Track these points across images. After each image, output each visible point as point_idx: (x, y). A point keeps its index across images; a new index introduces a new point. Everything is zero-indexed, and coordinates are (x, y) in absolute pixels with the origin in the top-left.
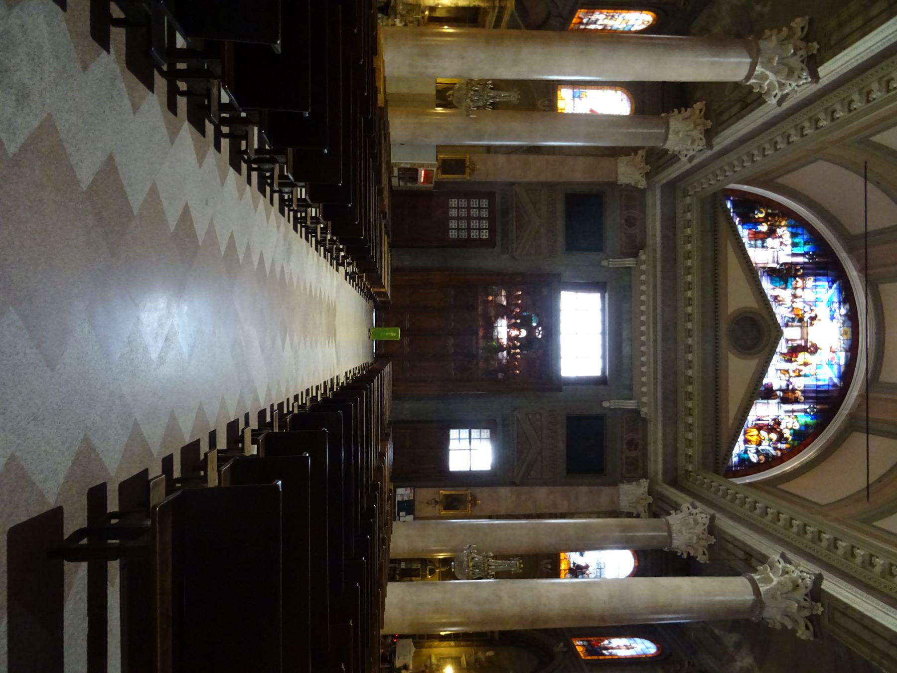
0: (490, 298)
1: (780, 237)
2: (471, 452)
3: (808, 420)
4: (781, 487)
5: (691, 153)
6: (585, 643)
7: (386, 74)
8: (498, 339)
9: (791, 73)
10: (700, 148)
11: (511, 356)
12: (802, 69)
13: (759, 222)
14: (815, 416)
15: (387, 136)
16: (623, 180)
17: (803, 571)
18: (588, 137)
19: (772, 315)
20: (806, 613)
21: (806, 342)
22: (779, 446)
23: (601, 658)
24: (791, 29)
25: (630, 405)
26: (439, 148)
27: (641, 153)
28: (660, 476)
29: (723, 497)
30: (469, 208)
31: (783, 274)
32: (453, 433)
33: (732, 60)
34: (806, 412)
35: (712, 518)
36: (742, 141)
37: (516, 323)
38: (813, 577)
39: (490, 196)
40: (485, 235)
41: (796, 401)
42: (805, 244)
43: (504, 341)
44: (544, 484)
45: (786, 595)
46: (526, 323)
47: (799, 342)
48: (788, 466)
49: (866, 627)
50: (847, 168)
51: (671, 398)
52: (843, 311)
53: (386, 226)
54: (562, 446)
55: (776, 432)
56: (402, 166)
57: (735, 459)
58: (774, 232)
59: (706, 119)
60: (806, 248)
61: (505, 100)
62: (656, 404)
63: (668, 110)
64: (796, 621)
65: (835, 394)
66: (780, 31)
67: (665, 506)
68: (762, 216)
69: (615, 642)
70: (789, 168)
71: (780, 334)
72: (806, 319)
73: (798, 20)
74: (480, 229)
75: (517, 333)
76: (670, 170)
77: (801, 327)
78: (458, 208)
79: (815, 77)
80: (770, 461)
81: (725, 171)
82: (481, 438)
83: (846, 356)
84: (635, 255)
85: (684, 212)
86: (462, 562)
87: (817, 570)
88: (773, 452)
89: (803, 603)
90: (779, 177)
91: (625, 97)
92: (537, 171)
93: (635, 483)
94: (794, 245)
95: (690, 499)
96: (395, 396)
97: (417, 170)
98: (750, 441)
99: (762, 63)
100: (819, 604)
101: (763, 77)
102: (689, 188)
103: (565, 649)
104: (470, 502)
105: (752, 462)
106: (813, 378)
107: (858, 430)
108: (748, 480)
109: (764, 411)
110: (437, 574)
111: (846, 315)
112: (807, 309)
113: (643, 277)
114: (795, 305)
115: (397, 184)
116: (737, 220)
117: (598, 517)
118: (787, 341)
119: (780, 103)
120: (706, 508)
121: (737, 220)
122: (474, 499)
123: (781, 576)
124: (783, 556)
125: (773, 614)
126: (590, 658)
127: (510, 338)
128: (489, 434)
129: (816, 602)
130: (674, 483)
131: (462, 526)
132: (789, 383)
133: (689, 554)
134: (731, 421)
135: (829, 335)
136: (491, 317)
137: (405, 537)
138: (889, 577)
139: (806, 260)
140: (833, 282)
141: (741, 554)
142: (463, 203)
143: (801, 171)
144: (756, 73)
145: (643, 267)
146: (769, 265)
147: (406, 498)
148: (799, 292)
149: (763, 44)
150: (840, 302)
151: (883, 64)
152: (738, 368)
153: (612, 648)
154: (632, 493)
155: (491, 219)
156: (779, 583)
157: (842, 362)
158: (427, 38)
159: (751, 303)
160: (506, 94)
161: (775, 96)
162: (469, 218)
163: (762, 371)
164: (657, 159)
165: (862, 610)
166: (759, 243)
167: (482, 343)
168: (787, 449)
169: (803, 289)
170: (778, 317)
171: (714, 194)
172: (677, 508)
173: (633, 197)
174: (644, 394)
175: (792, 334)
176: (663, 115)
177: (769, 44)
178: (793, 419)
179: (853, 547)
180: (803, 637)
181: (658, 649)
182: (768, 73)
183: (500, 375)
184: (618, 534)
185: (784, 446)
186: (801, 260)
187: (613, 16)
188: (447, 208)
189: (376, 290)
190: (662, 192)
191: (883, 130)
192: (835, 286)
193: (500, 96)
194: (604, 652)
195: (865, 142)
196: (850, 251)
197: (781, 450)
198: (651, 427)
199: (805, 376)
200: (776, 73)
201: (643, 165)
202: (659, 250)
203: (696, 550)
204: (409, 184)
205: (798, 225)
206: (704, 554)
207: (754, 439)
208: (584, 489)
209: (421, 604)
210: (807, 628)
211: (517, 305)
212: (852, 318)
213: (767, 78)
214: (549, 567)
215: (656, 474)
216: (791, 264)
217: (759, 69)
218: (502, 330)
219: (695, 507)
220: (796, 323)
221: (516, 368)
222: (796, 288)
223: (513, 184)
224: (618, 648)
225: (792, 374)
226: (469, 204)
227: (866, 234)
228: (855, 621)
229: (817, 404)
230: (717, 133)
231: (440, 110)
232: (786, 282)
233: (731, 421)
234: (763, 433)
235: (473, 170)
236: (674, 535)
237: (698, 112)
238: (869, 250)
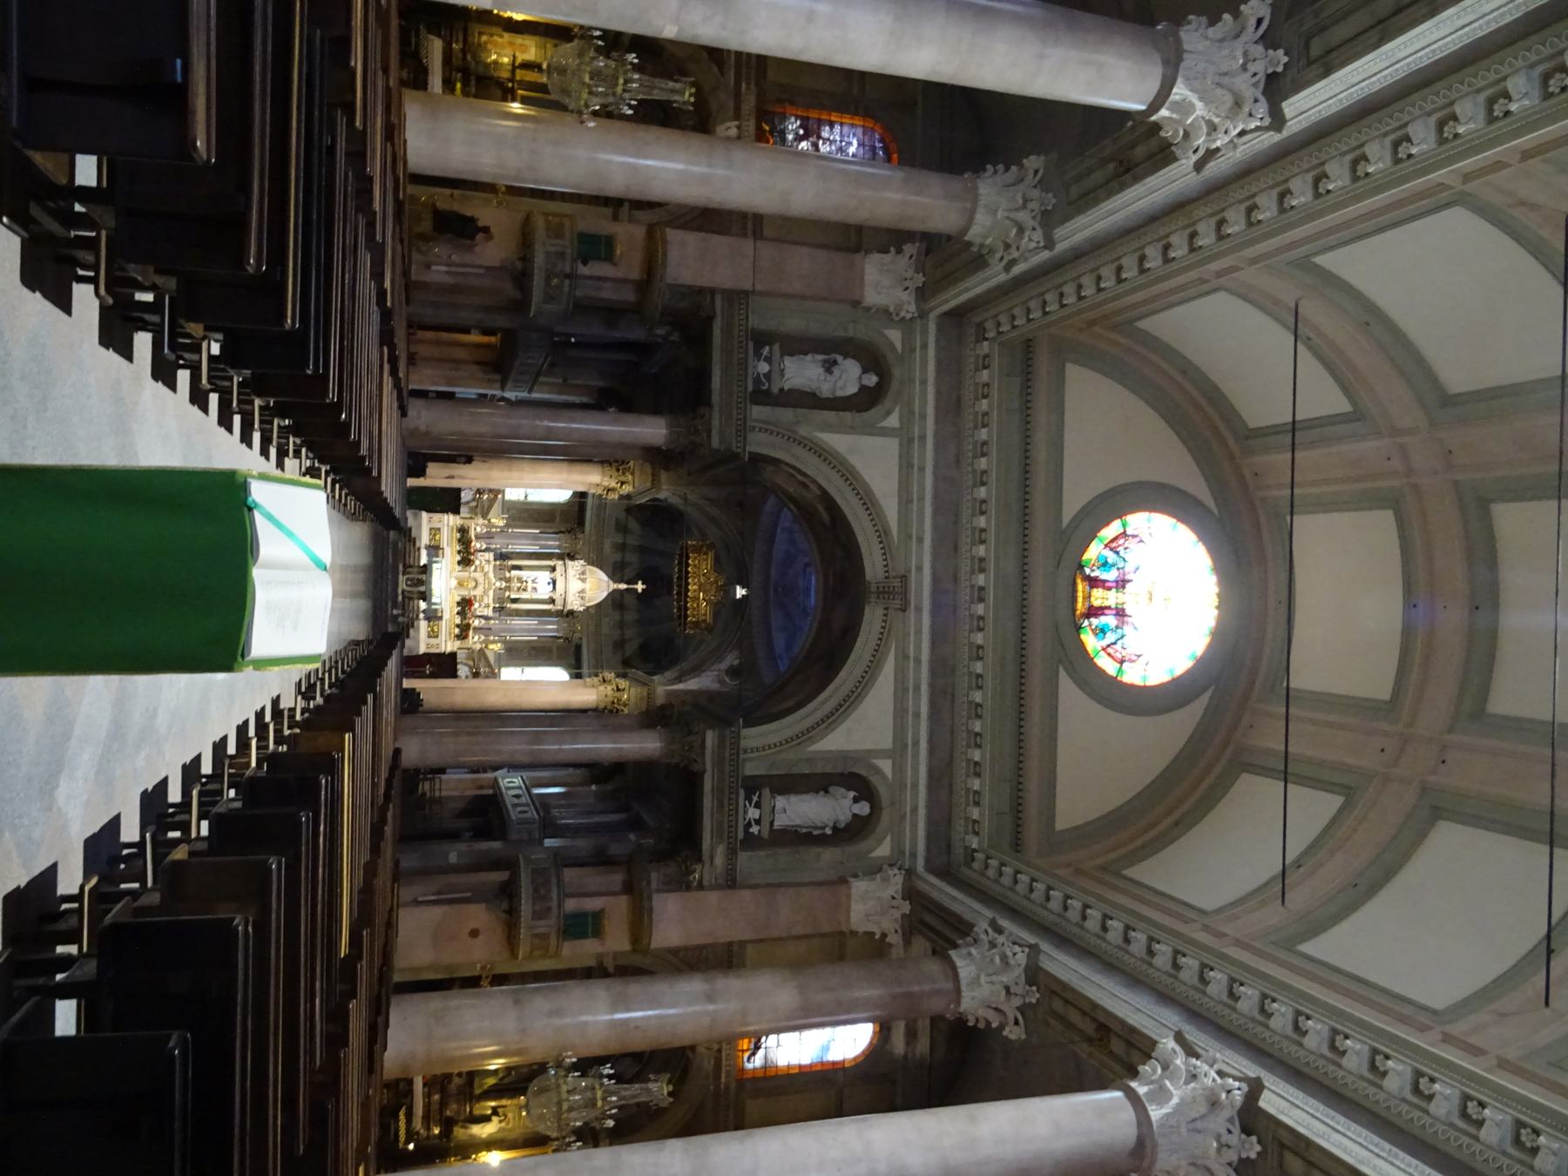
12: (1256, 101)
36: (1126, 233)
45: (1194, 1126)
63: (978, 169)
87: (1253, 1071)
90: (1139, 319)
95: (989, 914)
99: (1187, 79)
100: (1254, 1139)
101: (1184, 108)
119: (1199, 166)
123: (1186, 1083)
129: (1249, 1134)
144: (1172, 97)
156: (1182, 1099)
161: (1195, 151)
190: (939, 330)
195: (1306, 265)
206: (1017, 1023)
213: (1192, 108)
217: (1180, 91)
227: (1294, 426)
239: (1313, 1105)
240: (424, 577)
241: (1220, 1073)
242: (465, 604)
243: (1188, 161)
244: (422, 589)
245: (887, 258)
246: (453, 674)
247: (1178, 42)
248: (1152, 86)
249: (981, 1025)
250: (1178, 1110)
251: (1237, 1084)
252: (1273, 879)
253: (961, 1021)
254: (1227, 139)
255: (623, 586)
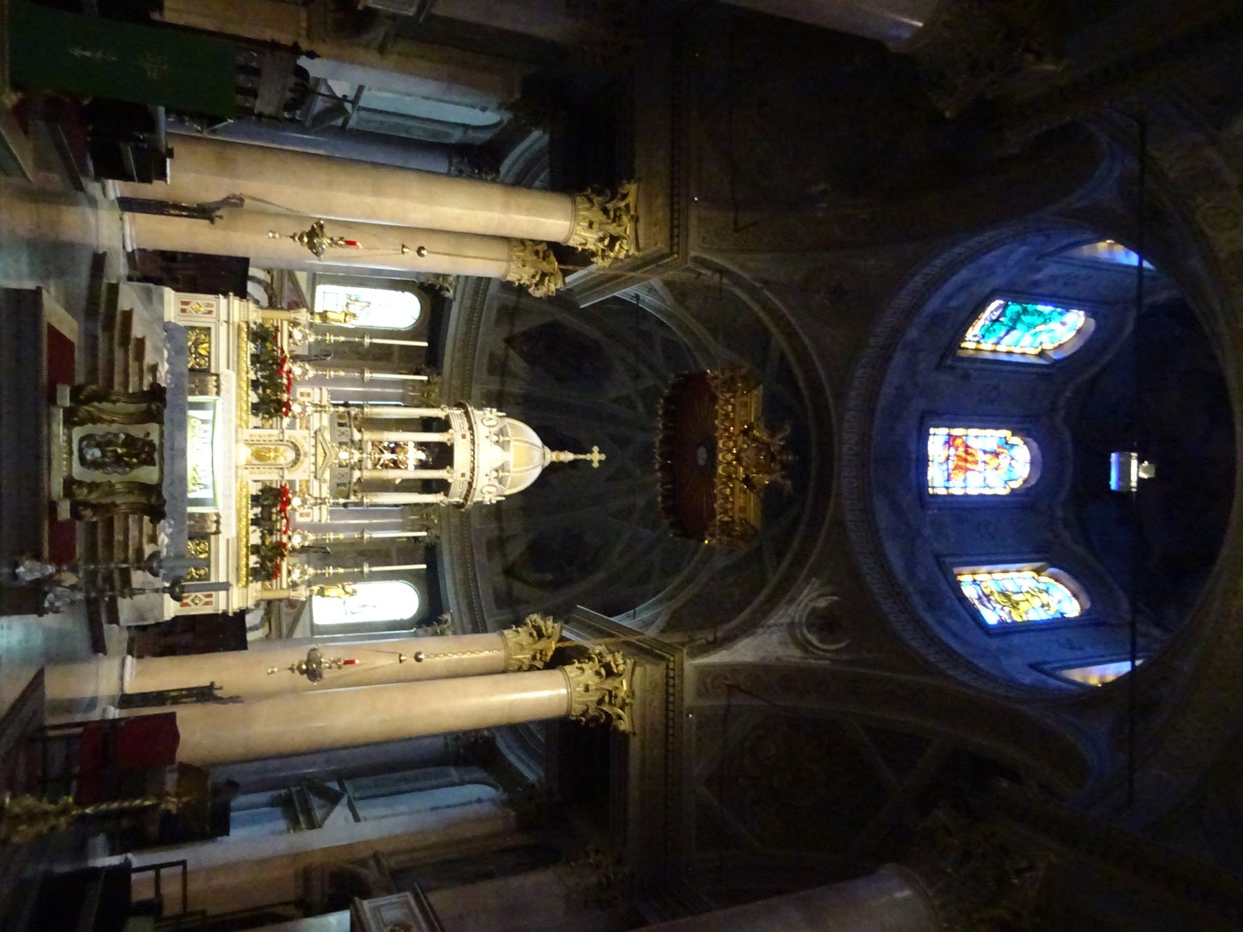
240: (153, 431)
242: (271, 502)
244: (148, 474)
246: (240, 644)
255: (567, 456)
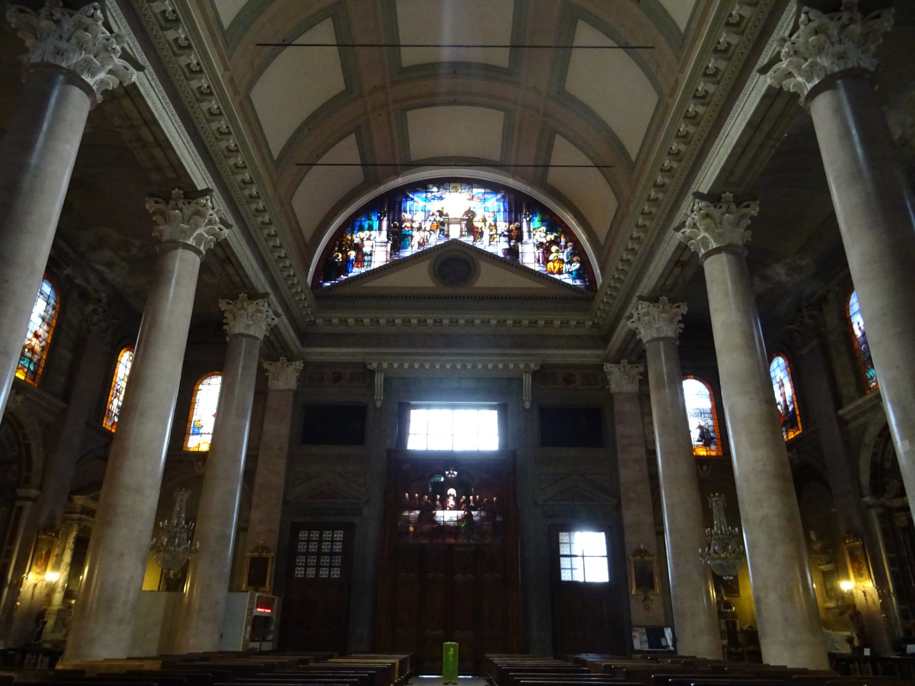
0: (411, 529)
1: (362, 240)
2: (586, 557)
3: (537, 219)
4: (634, 159)
5: (271, 313)
6: (784, 429)
7: (123, 655)
8: (458, 521)
9: (199, 213)
10: (266, 305)
11: (478, 506)
13: (347, 259)
14: (534, 214)
15: (206, 656)
16: (293, 384)
17: (691, 211)
18: (241, 417)
19: (437, 248)
20: (733, 207)
21: (463, 220)
22: (563, 243)
23: (798, 413)
24: (154, 213)
25: (527, 380)
26: (233, 588)
27: (266, 365)
28: (600, 352)
29: (622, 282)
30: (307, 554)
31: (398, 238)
32: (566, 576)
33: (177, 265)
34: (530, 221)
35: (641, 298)
36: (264, 266)
37: (440, 500)
38: (697, 200)
39: (295, 529)
40: (339, 535)
41: (520, 229)
42: (370, 220)
43: (461, 513)
44: (616, 471)
46: (441, 489)
47: (463, 226)
48: (583, 237)
49: (743, 152)
50: (301, 181)
51: (519, 341)
52: (435, 189)
53: (316, 661)
54: (573, 452)
55: (550, 246)
56: (248, 637)
57: (578, 283)
58: (357, 245)
59: (237, 298)
60: (374, 218)
61: (184, 507)
62: (526, 355)
63: (224, 334)
64: (742, 217)
65: (512, 197)
66: (156, 223)
67: (631, 346)
68: (340, 256)
69: (779, 399)
70: (297, 230)
71: (455, 241)
72: (442, 220)
73: (147, 207)
74: (332, 541)
75: (451, 498)
76: (286, 335)
77: (449, 224)
78: (306, 567)
79: (207, 192)
80: (578, 251)
81: (289, 276)
82: (570, 543)
83: (477, 187)
84: (372, 373)
85: (332, 325)
86: (721, 566)
87: (690, 197)
88: (569, 249)
89: (724, 209)
91: (206, 381)
92: (273, 473)
93: (609, 377)
94: (371, 228)
95: (623, 321)
96: (525, 650)
97: (256, 617)
98: (559, 269)
100: (723, 195)
101: (200, 238)
102: (307, 320)
103: (794, 450)
104: (642, 557)
105: (580, 267)
106: (498, 215)
107: (545, 174)
108: (597, 271)
109: (529, 256)
110: (730, 599)
111: (438, 188)
112: (432, 218)
113: (396, 365)
114: (428, 229)
115: (270, 644)
116: (343, 277)
117: (650, 414)
118: (462, 235)
119: (228, 226)
120: (631, 306)
121: (343, 277)
122: (638, 552)
123: (698, 229)
124: (677, 229)
125: (738, 236)
126: (800, 424)
127: (457, 507)
128: (564, 534)
129: (721, 198)
130: (605, 339)
131: (676, 566)
132: (502, 235)
133: (680, 322)
134: (542, 286)
135: (456, 202)
136: (433, 529)
137: (697, 640)
138: (689, 138)
139: (386, 219)
140: (407, 197)
141: (677, 270)
142: (301, 560)
143: (299, 218)
145: (385, 365)
146: (389, 250)
147: (645, 638)
148: (416, 225)
149: (166, 237)
150: (426, 192)
151: (204, 137)
152: (488, 279)
153: (785, 401)
154: (620, 380)
155: (322, 527)
156: (706, 230)
157: (482, 191)
158: (90, 600)
159: (424, 266)
160: (178, 505)
162: (319, 554)
163: (492, 257)
164: (274, 348)
165: (726, 156)
166: (366, 258)
167: (462, 540)
168: (565, 237)
169: (413, 222)
170: (438, 243)
171: (316, 297)
172: (633, 334)
173: (312, 374)
174: (516, 366)
175: (455, 232)
176: (228, 340)
177: (167, 231)
178: (536, 232)
179: (728, 24)
180: (758, 209)
181: (778, 355)
182: (195, 234)
183: (499, 519)
184: (667, 390)
185: (563, 240)
186: (385, 223)
187: (117, 391)
188: (305, 579)
189: (397, 675)
191: (269, 150)
192: (411, 196)
193: (180, 512)
194: (790, 409)
196: (378, 182)
197: (566, 243)
198: (551, 360)
199: (495, 221)
200: (197, 227)
201: (279, 364)
202: (366, 350)
203: (675, 315)
204: (272, 628)
205: (352, 224)
206: (678, 307)
207: (557, 265)
208: (620, 429)
209: (786, 619)
210: (748, 206)
211: (421, 497)
212: (441, 183)
213: (201, 234)
214: (705, 467)
215: (598, 356)
216: (388, 231)
217: (191, 241)
218: (448, 516)
219: (631, 316)
220: (446, 228)
221: (490, 501)
222: (412, 228)
223: (285, 503)
224: (783, 394)
225: (494, 232)
226: (302, 554)
227: (364, 165)
228: (771, 105)
229: (521, 212)
230: (253, 288)
231: (187, 587)
232: (407, 236)
233: (542, 286)
234: (551, 257)
235: (265, 548)
236: (662, 335)
237: (230, 307)
238: (379, 163)
239: (743, 97)
241: (692, 211)
243: (135, 77)
245: (270, 376)
247: (167, 242)
248: (77, 94)
249: (682, 326)
250: (712, 233)
251: (803, 16)
252: (602, 172)
253: (681, 336)
254: (215, 215)
